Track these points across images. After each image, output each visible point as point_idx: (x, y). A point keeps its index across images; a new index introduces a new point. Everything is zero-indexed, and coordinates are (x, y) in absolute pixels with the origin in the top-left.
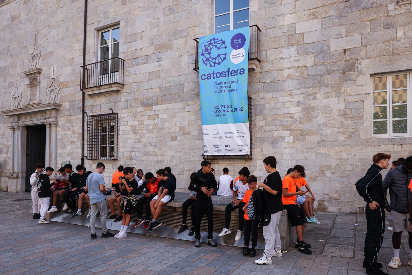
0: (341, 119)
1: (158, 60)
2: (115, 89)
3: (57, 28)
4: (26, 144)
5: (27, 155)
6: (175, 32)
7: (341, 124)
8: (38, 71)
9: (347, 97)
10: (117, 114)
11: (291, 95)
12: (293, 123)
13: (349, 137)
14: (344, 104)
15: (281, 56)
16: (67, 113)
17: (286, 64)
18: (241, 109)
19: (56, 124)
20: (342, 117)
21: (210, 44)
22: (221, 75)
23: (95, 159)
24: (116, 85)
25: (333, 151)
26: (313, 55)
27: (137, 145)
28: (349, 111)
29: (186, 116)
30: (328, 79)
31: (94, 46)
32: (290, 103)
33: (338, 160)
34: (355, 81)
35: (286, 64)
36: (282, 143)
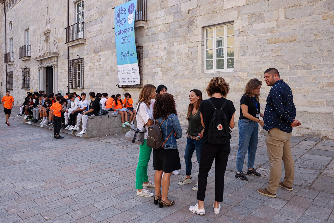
0: (186, 59)
1: (100, 22)
2: (80, 42)
3: (57, 3)
4: (46, 79)
5: (47, 86)
6: (108, 3)
7: (186, 63)
8: (48, 31)
9: (189, 44)
10: (83, 58)
11: (161, 43)
12: (162, 63)
13: (190, 73)
14: (188, 49)
15: (157, 16)
16: (62, 59)
17: (159, 22)
18: (132, 54)
19: (57, 66)
20: (187, 58)
21: (119, 12)
22: (124, 32)
23: (74, 88)
24: (81, 40)
25: (182, 82)
26: (173, 15)
27: (92, 79)
28: (190, 53)
29: (113, 59)
30: (180, 32)
31: (73, 14)
32: (161, 49)
33: (184, 88)
34: (194, 32)
35: (159, 22)
36: (157, 76)
